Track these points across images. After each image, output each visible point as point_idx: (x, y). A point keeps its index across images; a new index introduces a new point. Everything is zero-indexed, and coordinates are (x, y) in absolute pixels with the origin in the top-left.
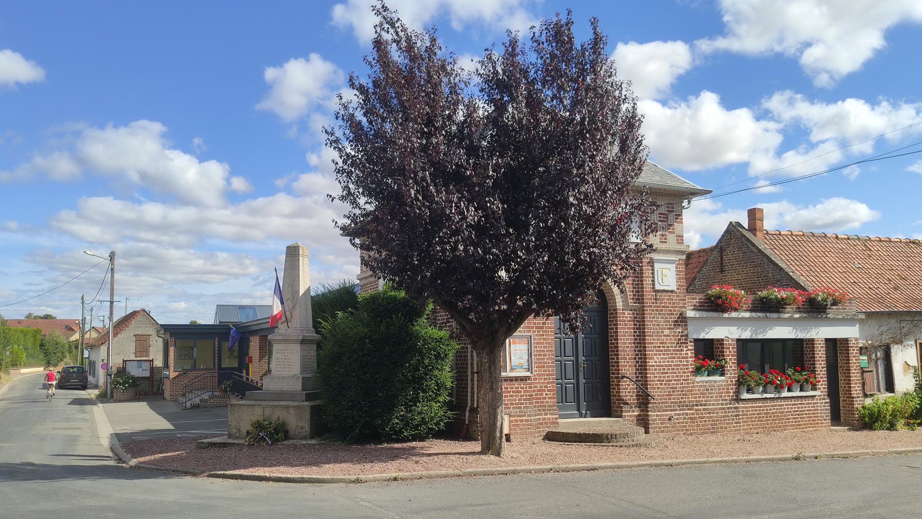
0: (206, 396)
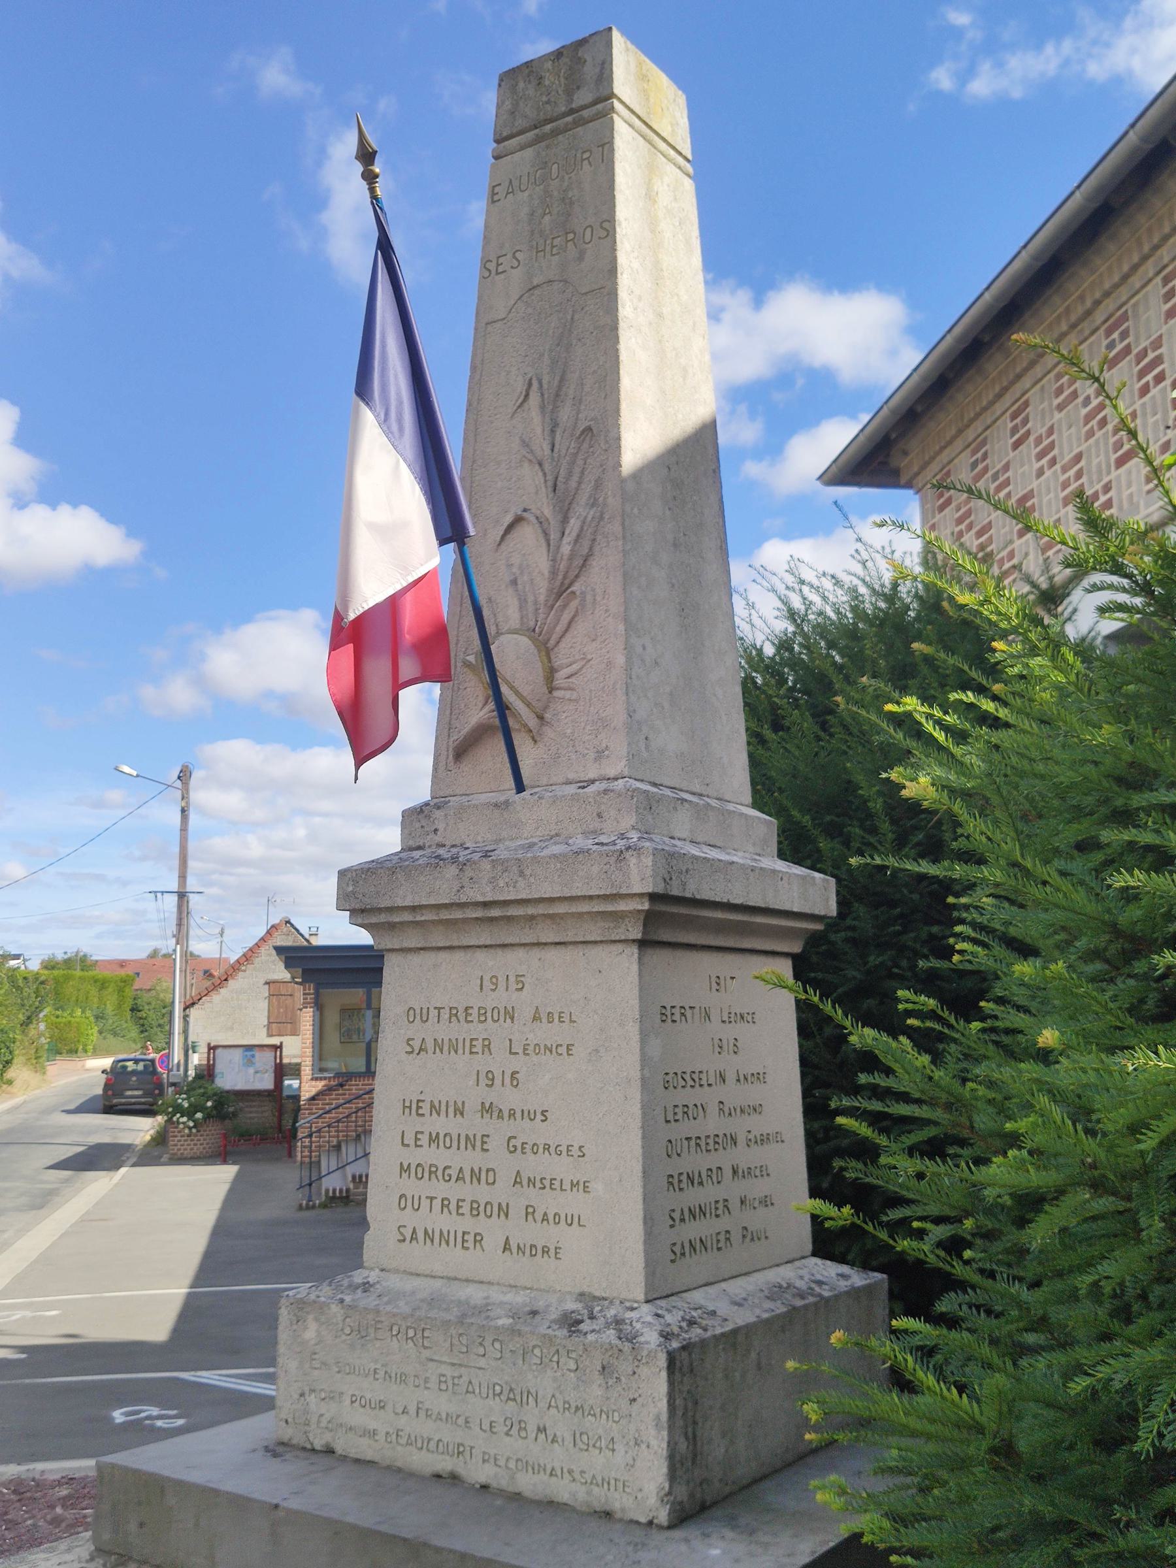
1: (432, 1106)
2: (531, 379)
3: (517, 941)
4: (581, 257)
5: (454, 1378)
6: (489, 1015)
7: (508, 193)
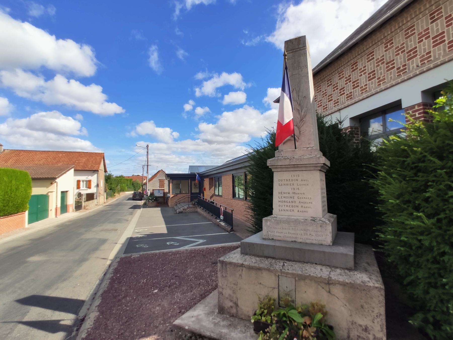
0: (186, 207)
4: (302, 71)
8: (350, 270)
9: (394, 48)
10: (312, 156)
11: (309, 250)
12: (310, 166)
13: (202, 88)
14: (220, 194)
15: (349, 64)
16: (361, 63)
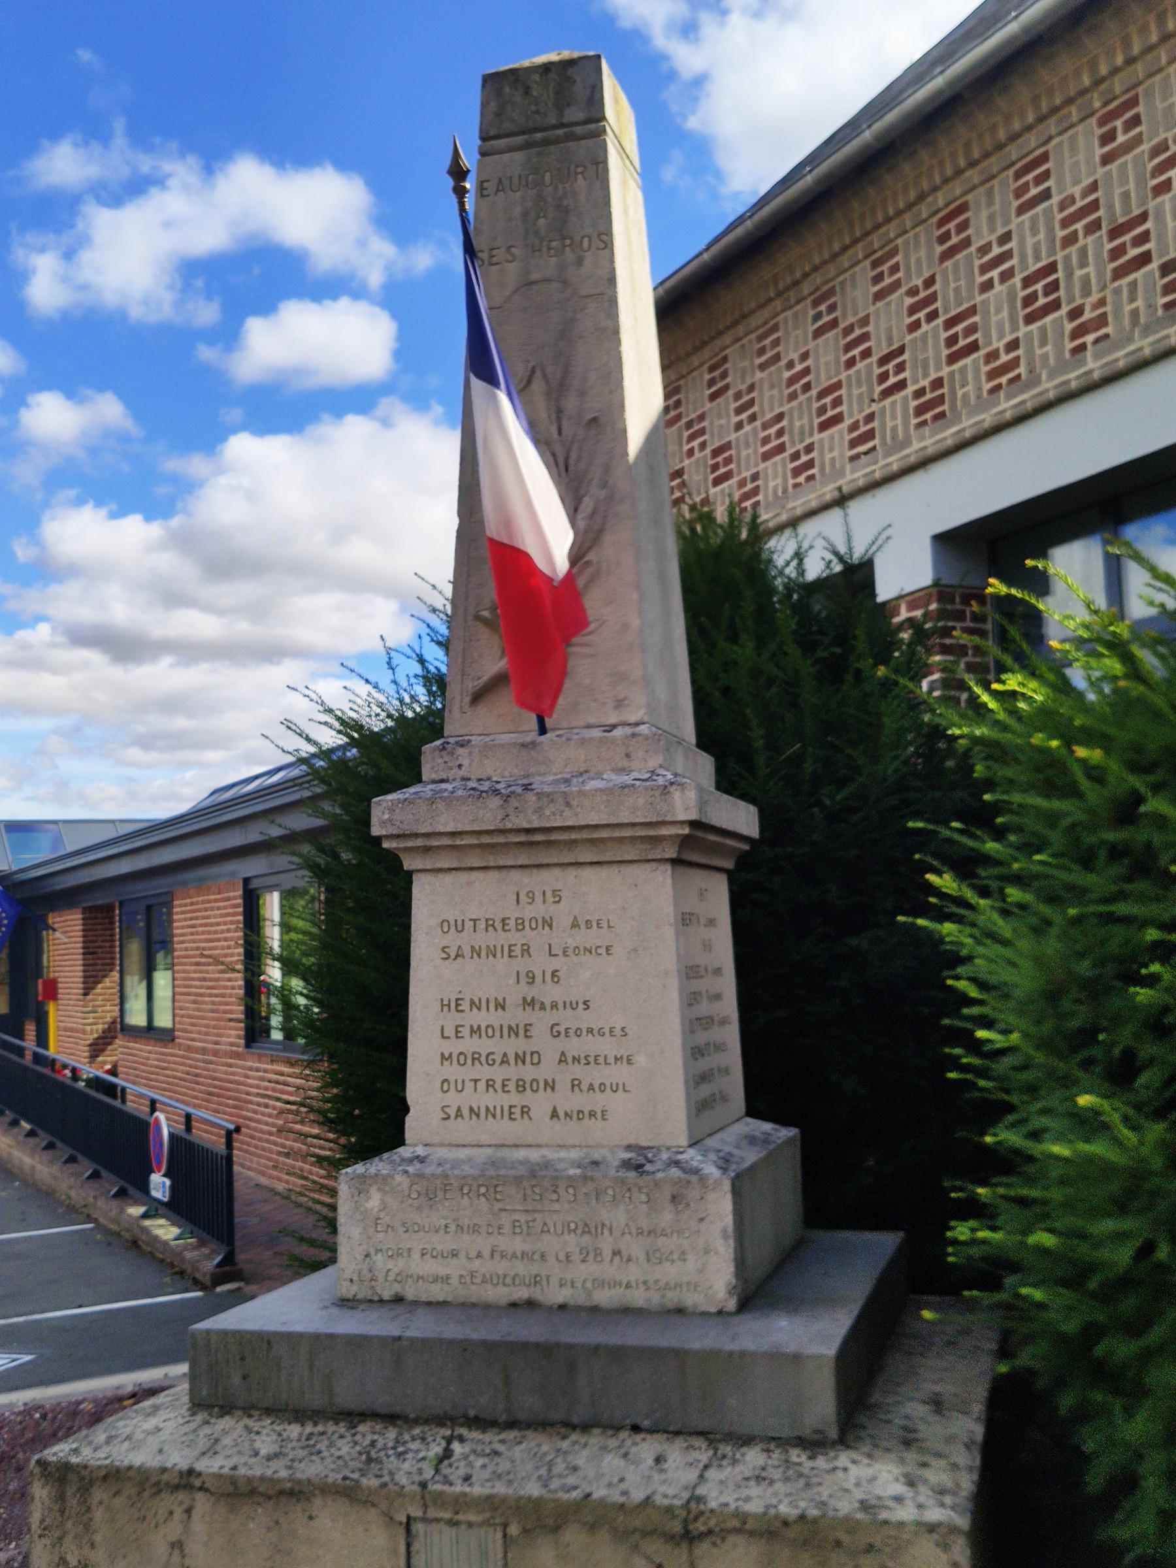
1: (472, 1003)
2: (534, 367)
3: (556, 861)
4: (580, 262)
5: (527, 1222)
6: (527, 924)
7: (498, 190)
8: (814, 1444)
9: (1145, 147)
10: (626, 779)
11: (596, 1349)
12: (621, 840)
13: (86, 256)
14: (163, 1020)
15: (924, 210)
16: (984, 214)
